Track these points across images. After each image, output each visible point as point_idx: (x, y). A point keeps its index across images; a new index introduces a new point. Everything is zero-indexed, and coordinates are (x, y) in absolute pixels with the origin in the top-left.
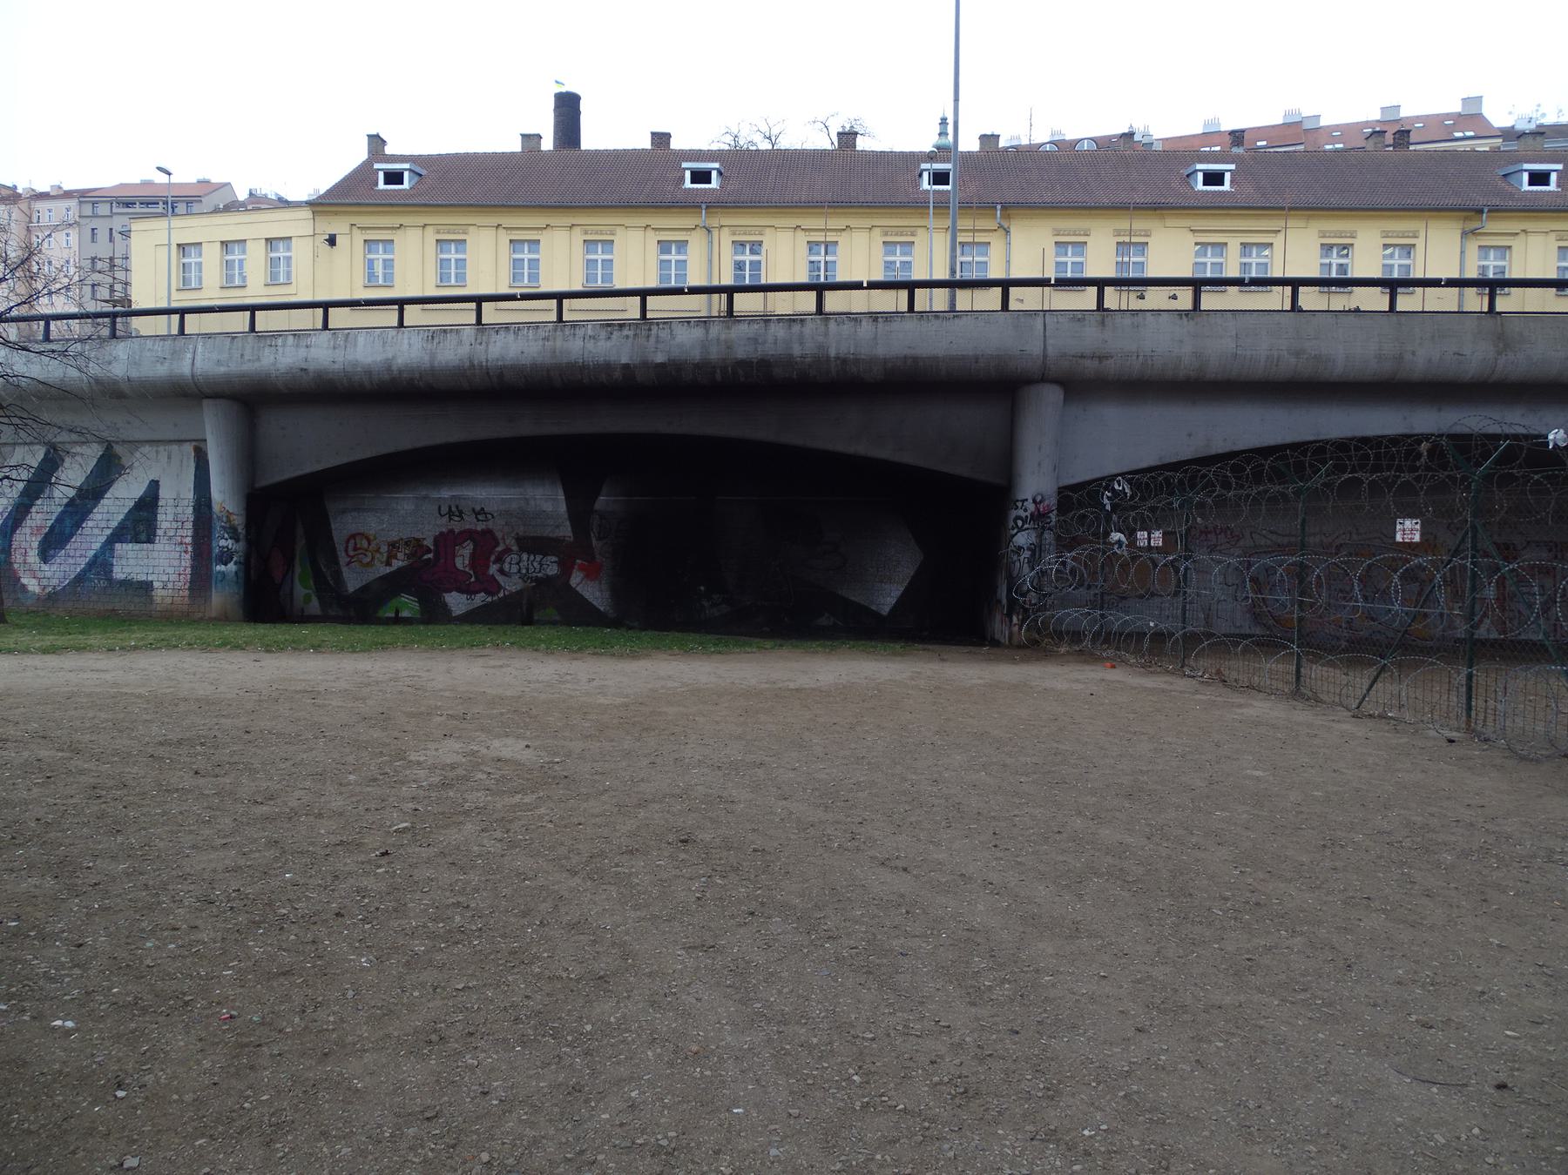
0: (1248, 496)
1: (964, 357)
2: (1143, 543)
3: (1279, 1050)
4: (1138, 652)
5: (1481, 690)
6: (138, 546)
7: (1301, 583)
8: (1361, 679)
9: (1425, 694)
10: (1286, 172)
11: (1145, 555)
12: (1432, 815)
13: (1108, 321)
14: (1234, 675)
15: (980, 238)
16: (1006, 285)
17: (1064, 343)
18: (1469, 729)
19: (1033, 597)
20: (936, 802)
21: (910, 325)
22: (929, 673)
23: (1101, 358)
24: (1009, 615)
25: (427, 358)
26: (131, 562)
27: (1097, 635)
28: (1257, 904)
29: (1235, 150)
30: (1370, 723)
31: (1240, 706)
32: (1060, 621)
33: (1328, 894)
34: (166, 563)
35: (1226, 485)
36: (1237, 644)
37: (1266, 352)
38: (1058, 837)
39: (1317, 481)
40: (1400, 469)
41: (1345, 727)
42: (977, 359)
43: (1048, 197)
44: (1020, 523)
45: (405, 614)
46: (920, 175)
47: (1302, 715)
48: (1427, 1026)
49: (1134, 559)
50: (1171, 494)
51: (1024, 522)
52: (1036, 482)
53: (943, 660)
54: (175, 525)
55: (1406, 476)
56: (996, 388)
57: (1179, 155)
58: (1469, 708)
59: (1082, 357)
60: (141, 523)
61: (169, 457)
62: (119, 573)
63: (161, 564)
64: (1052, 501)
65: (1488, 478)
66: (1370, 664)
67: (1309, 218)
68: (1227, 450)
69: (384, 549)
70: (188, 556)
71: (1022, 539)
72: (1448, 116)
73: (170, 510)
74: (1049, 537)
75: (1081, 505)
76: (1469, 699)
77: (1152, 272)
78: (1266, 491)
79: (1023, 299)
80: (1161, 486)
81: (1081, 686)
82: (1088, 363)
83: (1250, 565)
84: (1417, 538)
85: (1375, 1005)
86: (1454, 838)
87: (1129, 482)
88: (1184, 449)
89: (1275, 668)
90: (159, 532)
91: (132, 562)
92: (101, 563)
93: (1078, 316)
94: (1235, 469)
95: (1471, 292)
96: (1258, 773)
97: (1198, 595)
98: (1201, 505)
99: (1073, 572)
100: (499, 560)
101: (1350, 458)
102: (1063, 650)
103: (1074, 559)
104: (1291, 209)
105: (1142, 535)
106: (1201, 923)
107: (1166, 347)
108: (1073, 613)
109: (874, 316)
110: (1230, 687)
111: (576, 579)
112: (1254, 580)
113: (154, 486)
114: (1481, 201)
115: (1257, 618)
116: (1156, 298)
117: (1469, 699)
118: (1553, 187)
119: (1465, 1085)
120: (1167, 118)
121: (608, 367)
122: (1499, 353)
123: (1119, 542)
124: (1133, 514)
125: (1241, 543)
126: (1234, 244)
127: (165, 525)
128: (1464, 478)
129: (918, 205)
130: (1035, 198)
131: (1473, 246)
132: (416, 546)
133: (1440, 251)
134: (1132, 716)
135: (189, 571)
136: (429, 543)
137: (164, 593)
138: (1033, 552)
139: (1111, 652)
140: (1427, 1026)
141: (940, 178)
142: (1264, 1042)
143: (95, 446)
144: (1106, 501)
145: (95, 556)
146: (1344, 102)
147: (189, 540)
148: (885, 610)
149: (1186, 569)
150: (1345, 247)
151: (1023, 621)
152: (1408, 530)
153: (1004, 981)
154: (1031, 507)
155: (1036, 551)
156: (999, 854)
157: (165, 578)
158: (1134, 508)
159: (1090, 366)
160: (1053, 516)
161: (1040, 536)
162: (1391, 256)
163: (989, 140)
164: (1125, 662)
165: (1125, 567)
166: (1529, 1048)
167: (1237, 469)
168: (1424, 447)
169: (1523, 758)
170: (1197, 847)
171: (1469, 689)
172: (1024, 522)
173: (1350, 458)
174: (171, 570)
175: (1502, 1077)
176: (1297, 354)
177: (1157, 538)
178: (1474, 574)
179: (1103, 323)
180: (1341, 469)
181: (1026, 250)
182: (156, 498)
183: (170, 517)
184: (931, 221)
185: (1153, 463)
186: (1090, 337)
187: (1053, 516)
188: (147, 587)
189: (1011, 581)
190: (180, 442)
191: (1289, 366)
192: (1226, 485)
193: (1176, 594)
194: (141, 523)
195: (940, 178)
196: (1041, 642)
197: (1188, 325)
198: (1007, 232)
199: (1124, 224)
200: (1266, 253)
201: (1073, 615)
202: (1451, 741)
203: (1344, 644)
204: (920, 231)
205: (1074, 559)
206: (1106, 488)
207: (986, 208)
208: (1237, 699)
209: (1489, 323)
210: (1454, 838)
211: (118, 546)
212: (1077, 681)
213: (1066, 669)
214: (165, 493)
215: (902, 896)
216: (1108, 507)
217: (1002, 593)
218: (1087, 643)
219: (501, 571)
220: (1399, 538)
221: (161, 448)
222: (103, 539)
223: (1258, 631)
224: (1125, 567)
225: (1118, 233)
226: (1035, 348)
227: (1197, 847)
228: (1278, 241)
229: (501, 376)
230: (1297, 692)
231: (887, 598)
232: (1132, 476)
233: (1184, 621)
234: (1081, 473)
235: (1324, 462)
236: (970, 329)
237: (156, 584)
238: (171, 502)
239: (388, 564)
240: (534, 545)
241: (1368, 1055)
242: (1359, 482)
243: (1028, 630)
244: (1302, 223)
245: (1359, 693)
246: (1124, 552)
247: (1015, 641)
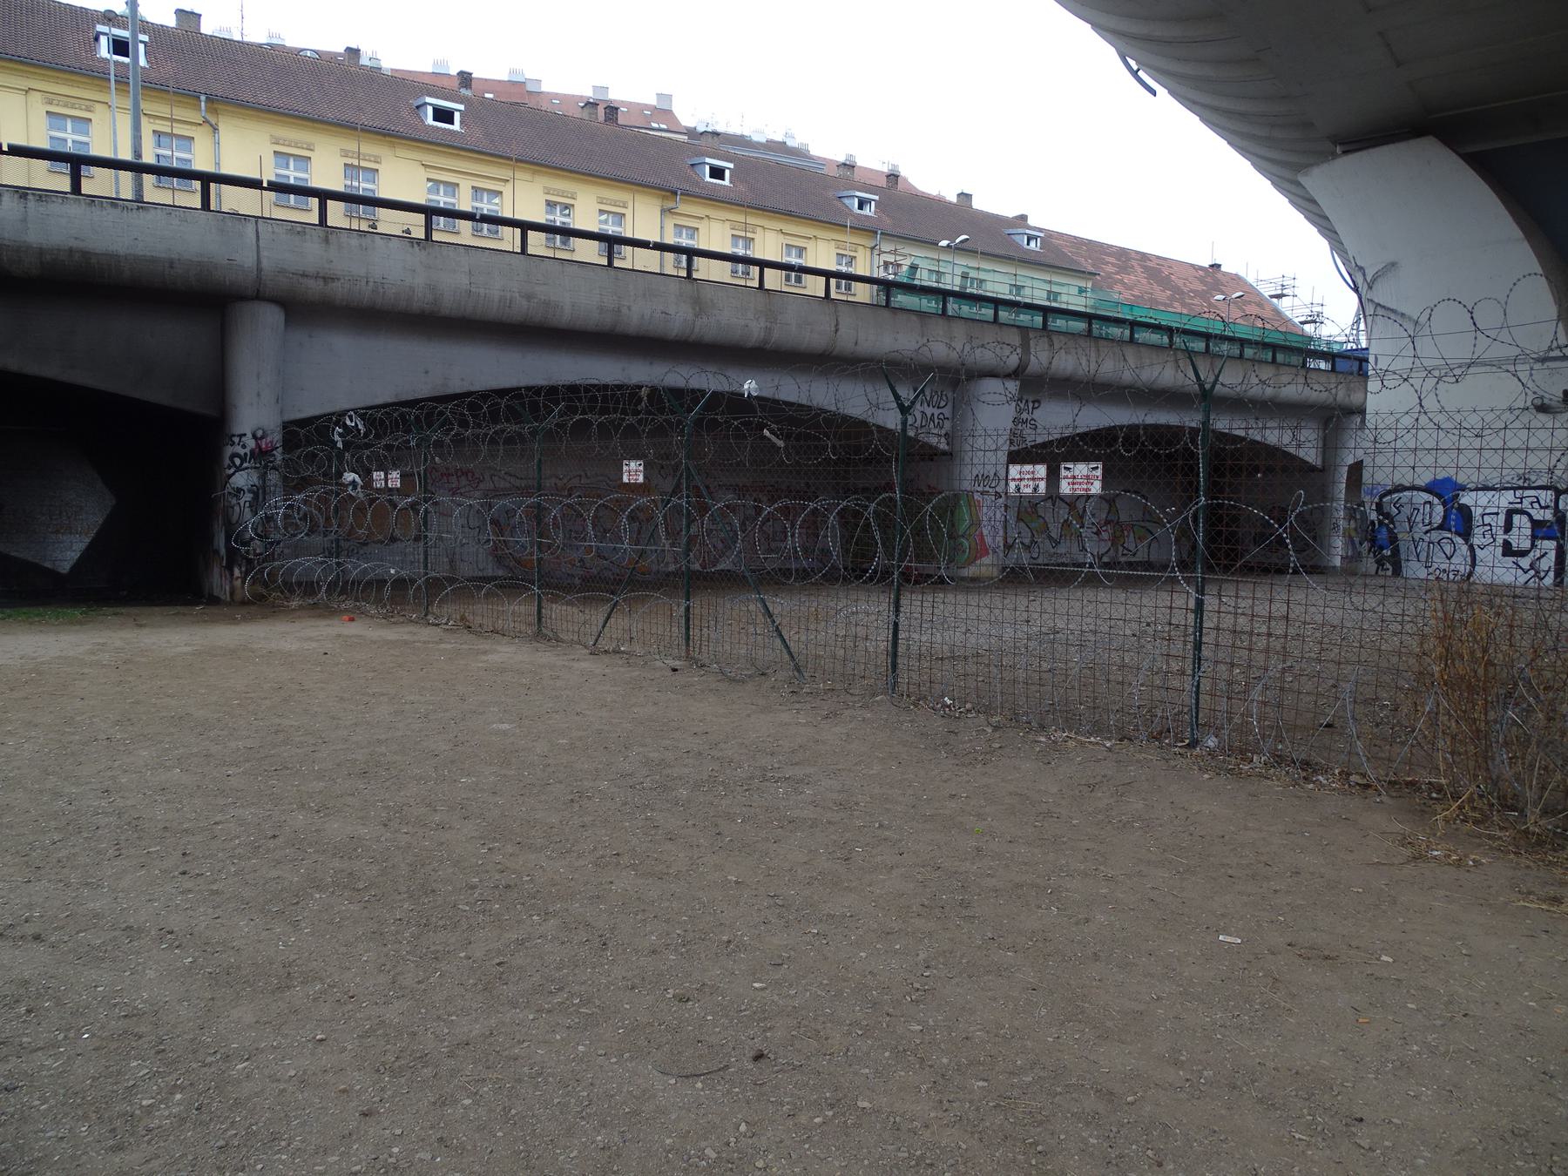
0: (486, 435)
1: (153, 260)
2: (379, 485)
3: (536, 1087)
4: (379, 601)
5: (697, 622)
7: (539, 524)
8: (597, 615)
9: (649, 623)
10: (512, 126)
11: (383, 497)
12: (666, 749)
13: (332, 238)
14: (478, 620)
15: (180, 130)
16: (207, 179)
17: (280, 258)
18: (688, 657)
19: (257, 545)
20: (103, 821)
21: (75, 209)
22: (118, 643)
23: (326, 279)
24: (230, 568)
27: (332, 587)
28: (508, 887)
29: (463, 91)
30: (606, 659)
31: (485, 653)
32: (291, 571)
33: (579, 857)
35: (464, 424)
36: (480, 588)
37: (498, 292)
38: (272, 844)
39: (551, 421)
40: (624, 412)
41: (584, 665)
42: (171, 263)
43: (263, 98)
44: (238, 461)
46: (97, 39)
47: (545, 657)
48: (683, 999)
49: (372, 501)
50: (408, 431)
51: (243, 460)
52: (255, 414)
53: (141, 626)
55: (630, 419)
56: (205, 302)
57: (405, 87)
58: (688, 639)
59: (304, 275)
64: (276, 437)
65: (698, 423)
66: (605, 601)
67: (534, 172)
68: (465, 390)
71: (241, 480)
72: (647, 107)
74: (273, 477)
75: (309, 442)
76: (688, 629)
77: (384, 194)
78: (503, 431)
79: (231, 199)
80: (396, 425)
81: (314, 645)
82: (311, 283)
83: (491, 507)
84: (641, 479)
85: (633, 988)
86: (687, 771)
87: (363, 417)
88: (422, 387)
89: (518, 610)
93: (298, 229)
94: (472, 407)
95: (670, 256)
96: (506, 726)
97: (441, 539)
98: (439, 444)
99: (304, 519)
101: (580, 400)
102: (294, 604)
103: (305, 502)
104: (517, 160)
105: (378, 476)
106: (444, 927)
107: (396, 274)
108: (306, 561)
109: (22, 193)
110: (475, 633)
112: (495, 522)
114: (675, 184)
115: (499, 560)
116: (390, 222)
117: (688, 629)
118: (456, 127)
119: (727, 1067)
120: (399, 49)
122: (696, 316)
123: (354, 482)
124: (367, 452)
125: (482, 486)
126: (466, 186)
128: (679, 422)
129: (95, 75)
130: (247, 96)
131: (670, 223)
133: (644, 219)
134: (370, 675)
138: (256, 495)
139: (349, 604)
140: (683, 999)
141: (120, 47)
142: (519, 1081)
144: (337, 438)
146: (564, 76)
148: (65, 568)
149: (426, 510)
150: (567, 207)
151: (247, 573)
152: (633, 472)
153: (174, 1089)
154: (251, 444)
155: (259, 495)
156: (189, 885)
158: (368, 446)
159: (314, 287)
160: (278, 455)
161: (263, 477)
162: (606, 222)
163: (188, 18)
164: (364, 613)
165: (361, 509)
166: (776, 998)
167: (473, 407)
168: (644, 392)
169: (732, 680)
170: (441, 826)
171: (688, 620)
172: (243, 460)
173: (580, 400)
175: (758, 1044)
176: (529, 297)
177: (395, 479)
178: (689, 512)
179: (327, 240)
180: (572, 410)
181: (242, 148)
184: (113, 98)
185: (390, 400)
186: (312, 255)
187: (278, 455)
189: (230, 527)
191: (521, 309)
192: (464, 424)
193: (417, 539)
195: (120, 47)
196: (270, 595)
197: (419, 255)
198: (215, 129)
199: (352, 145)
200: (497, 200)
201: (309, 564)
202: (675, 670)
203: (577, 581)
204: (98, 106)
205: (305, 502)
206: (337, 424)
207: (188, 96)
208: (484, 645)
209: (688, 287)
210: (687, 771)
212: (310, 639)
213: (297, 626)
215: (25, 983)
216: (340, 445)
217: (220, 542)
218: (322, 594)
220: (625, 479)
223: (500, 573)
224: (361, 509)
225: (345, 153)
226: (247, 259)
227: (441, 826)
228: (507, 190)
230: (541, 633)
231: (67, 552)
232: (366, 413)
233: (426, 567)
234: (309, 408)
235: (557, 404)
236: (164, 228)
241: (632, 1058)
242: (588, 423)
243: (253, 583)
244: (527, 176)
245: (595, 630)
246: (359, 494)
247: (238, 597)
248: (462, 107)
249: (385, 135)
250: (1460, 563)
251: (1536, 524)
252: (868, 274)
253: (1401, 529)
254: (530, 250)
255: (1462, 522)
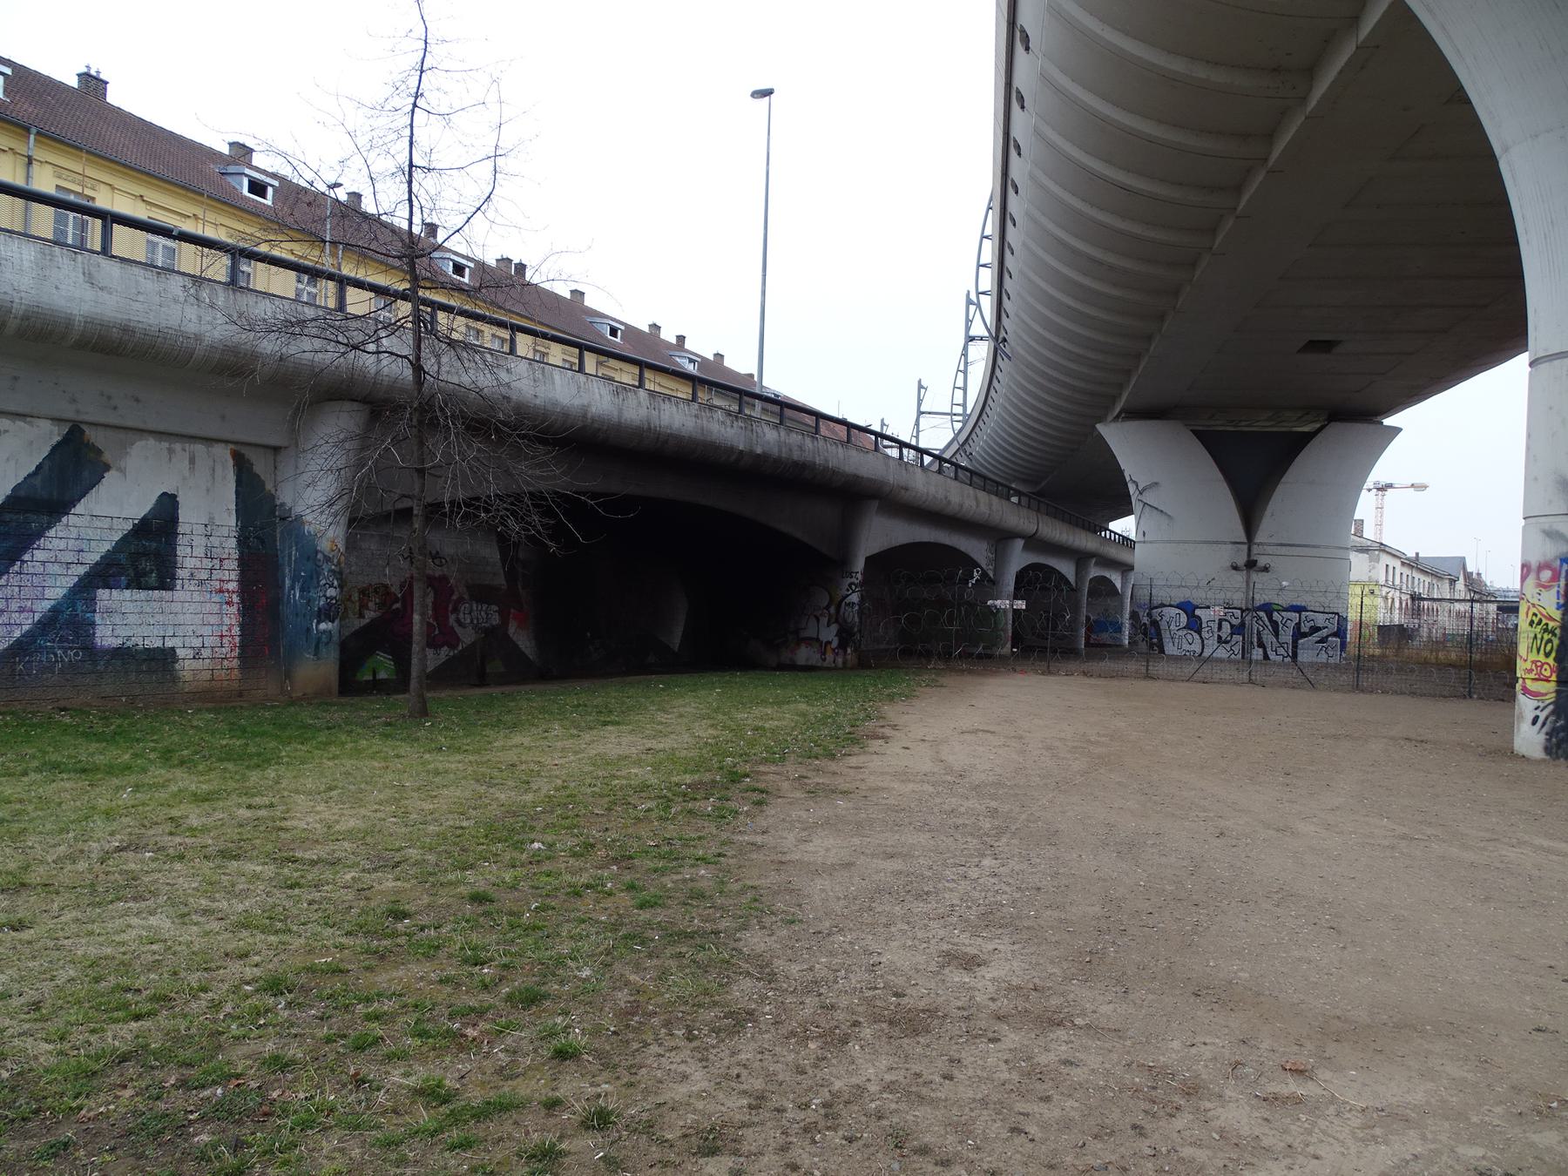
6: (143, 594)
25: (616, 413)
26: (125, 618)
34: (197, 619)
45: (382, 675)
54: (208, 563)
60: (147, 555)
61: (192, 461)
62: (107, 635)
63: (191, 621)
69: (356, 597)
70: (234, 609)
73: (200, 542)
90: (180, 573)
91: (132, 619)
92: (68, 622)
100: (456, 610)
111: (512, 629)
113: (168, 507)
121: (731, 450)
127: (190, 563)
132: (384, 592)
135: (236, 630)
136: (395, 589)
137: (198, 664)
143: (46, 425)
145: (55, 611)
147: (233, 586)
157: (197, 643)
174: (207, 631)
182: (174, 520)
183: (199, 551)
188: (163, 659)
190: (209, 441)
194: (147, 555)
211: (102, 594)
214: (189, 517)
219: (458, 621)
221: (178, 446)
222: (72, 581)
229: (584, 427)
231: (676, 640)
237: (180, 653)
238: (200, 530)
239: (361, 616)
240: (482, 594)
248: (276, 183)
249: (188, 189)
250: (1197, 647)
251: (1232, 626)
252: (35, 205)
253: (1163, 625)
254: (350, 309)
255: (1195, 625)
